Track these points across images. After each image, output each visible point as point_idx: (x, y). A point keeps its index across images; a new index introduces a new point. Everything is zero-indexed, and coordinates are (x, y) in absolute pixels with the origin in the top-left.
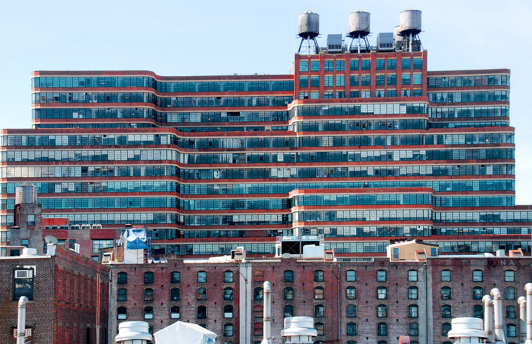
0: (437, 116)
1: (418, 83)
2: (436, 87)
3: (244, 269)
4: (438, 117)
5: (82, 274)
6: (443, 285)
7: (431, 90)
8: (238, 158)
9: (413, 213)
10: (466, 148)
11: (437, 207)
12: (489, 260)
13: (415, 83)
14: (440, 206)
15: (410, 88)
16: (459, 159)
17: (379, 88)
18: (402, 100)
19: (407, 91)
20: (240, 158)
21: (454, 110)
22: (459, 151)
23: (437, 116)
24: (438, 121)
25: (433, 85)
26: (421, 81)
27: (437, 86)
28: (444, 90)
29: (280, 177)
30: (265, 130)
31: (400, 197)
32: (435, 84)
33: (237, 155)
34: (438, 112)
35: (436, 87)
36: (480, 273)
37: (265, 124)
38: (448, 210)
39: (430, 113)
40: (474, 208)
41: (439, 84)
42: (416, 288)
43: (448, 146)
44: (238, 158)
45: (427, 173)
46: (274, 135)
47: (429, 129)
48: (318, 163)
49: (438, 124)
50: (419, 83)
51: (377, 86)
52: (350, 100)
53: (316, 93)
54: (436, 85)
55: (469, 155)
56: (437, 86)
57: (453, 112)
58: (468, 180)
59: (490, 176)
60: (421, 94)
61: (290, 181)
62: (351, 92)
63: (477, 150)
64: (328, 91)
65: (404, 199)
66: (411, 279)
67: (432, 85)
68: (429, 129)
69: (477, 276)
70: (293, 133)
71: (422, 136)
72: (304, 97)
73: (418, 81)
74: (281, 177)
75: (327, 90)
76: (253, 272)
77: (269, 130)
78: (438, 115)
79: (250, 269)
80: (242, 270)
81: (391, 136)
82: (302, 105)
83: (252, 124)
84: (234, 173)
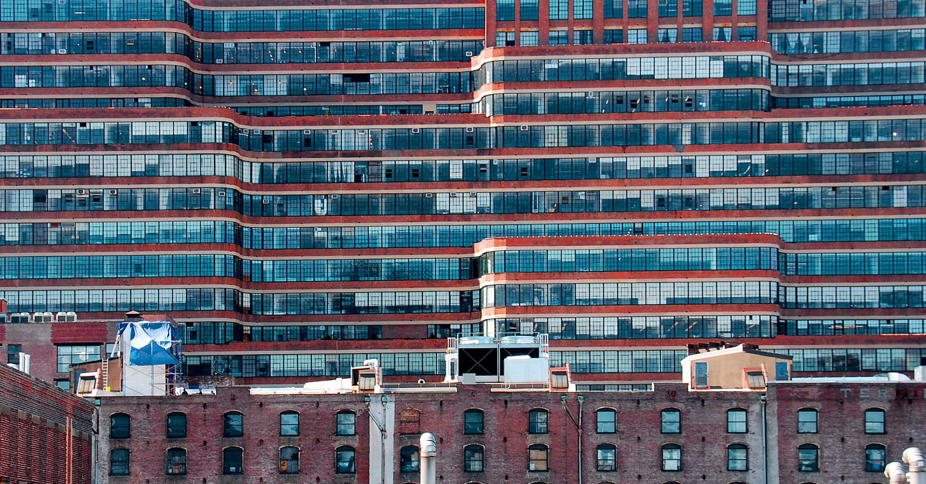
2: (786, 21)
3: (380, 407)
5: (36, 417)
6: (802, 440)
8: (366, 171)
9: (739, 288)
11: (790, 275)
12: (899, 387)
13: (742, 13)
14: (794, 273)
15: (731, 22)
20: (370, 172)
21: (824, 71)
22: (836, 158)
24: (791, 93)
25: (780, 16)
27: (788, 19)
29: (455, 212)
30: (424, 113)
31: (711, 253)
33: (364, 164)
34: (791, 74)
35: (786, 21)
36: (879, 416)
37: (424, 100)
41: (794, 15)
42: (745, 447)
44: (366, 171)
46: (442, 123)
47: (772, 110)
48: (536, 182)
51: (661, 20)
52: (603, 49)
56: (788, 19)
57: (822, 73)
58: (854, 217)
59: (901, 210)
60: (754, 36)
62: (606, 32)
63: (873, 155)
64: (558, 29)
65: (719, 259)
66: (733, 428)
69: (875, 423)
70: (483, 118)
71: (757, 124)
72: (506, 41)
73: (528, 38)
74: (458, 212)
75: (555, 27)
76: (398, 414)
77: (433, 112)
78: (790, 80)
79: (391, 407)
80: (375, 409)
82: (502, 58)
83: (397, 100)
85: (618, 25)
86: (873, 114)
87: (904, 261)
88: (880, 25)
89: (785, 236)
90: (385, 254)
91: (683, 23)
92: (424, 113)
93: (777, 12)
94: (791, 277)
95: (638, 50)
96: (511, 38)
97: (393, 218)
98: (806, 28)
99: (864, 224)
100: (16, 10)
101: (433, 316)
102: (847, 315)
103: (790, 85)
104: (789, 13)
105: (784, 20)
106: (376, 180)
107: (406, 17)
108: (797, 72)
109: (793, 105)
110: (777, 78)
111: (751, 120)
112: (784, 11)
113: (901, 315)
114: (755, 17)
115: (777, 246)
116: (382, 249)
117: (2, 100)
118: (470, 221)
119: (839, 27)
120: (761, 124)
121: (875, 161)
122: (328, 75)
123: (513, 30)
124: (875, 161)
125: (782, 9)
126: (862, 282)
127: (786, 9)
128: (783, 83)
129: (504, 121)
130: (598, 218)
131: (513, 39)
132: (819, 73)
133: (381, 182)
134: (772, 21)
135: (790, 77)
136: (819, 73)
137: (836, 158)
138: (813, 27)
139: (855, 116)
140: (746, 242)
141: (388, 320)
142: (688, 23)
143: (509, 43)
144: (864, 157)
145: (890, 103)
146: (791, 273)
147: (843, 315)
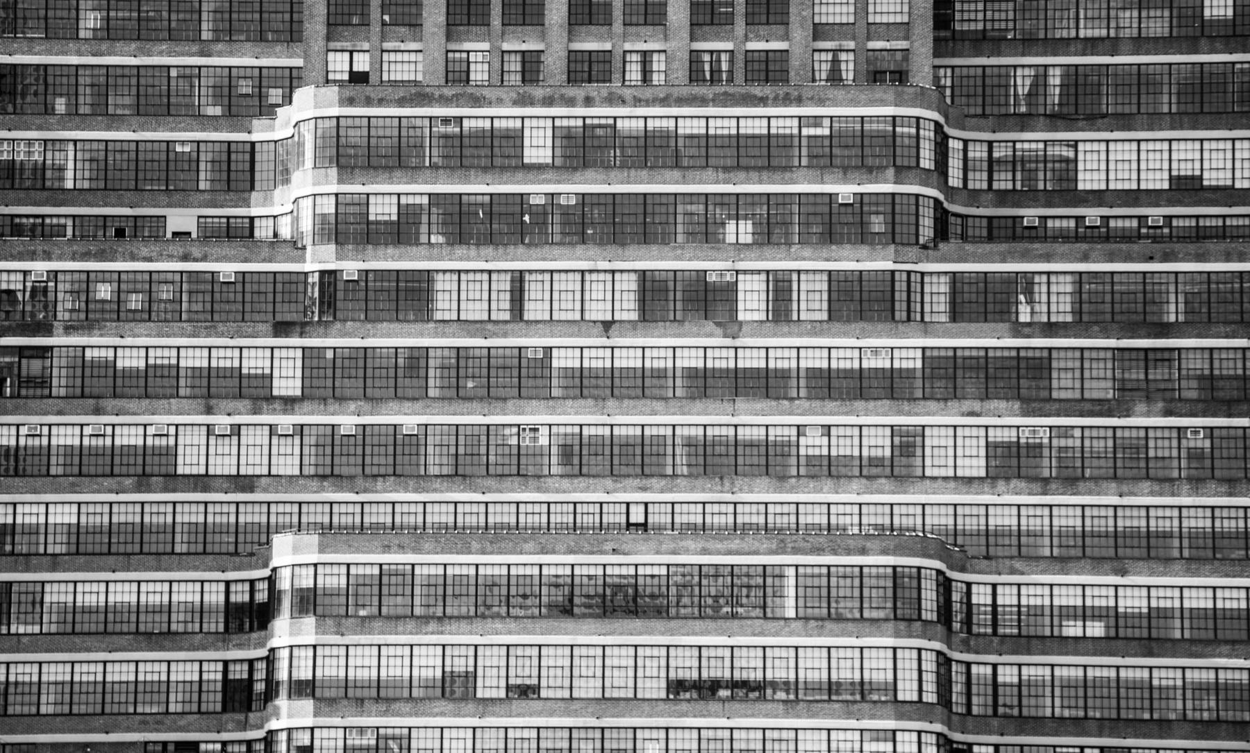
0: (990, 180)
1: (892, 19)
2: (984, 38)
4: (995, 186)
7: (961, 56)
8: (16, 371)
10: (1112, 343)
11: (979, 635)
13: (878, 19)
14: (989, 630)
15: (854, 38)
16: (1083, 399)
17: (705, 40)
18: (812, 99)
19: (843, 56)
20: (24, 373)
21: (1071, 155)
22: (1082, 359)
23: (990, 180)
24: (997, 206)
25: (973, 26)
26: (385, 67)
27: (989, 34)
28: (1023, 55)
29: (219, 472)
30: (169, 235)
32: (980, 26)
33: (12, 355)
34: (999, 161)
35: (984, 38)
37: (169, 206)
38: (1029, 653)
39: (955, 165)
40: (1154, 644)
41: (1003, 26)
43: (1026, 330)
44: (16, 371)
45: (834, 453)
46: (196, 260)
47: (941, 245)
48: (407, 404)
49: (995, 223)
50: (899, 19)
51: (698, 31)
52: (562, 96)
53: (406, 57)
54: (985, 30)
55: (1127, 376)
56: (989, 34)
57: (1067, 161)
58: (1127, 501)
61: (265, 490)
62: (573, 57)
63: (1166, 355)
64: (467, 46)
65: (801, 592)
67: (965, 27)
68: (941, 245)
70: (296, 246)
71: (904, 276)
72: (351, 72)
73: (399, 66)
74: (226, 472)
75: (460, 40)
77: (189, 234)
78: (996, 176)
81: (508, 277)
82: (336, 111)
83: (106, 205)
84: (1123, 691)
85: (601, 38)
86: (1166, 258)
87: (189, 311)
88: (1196, 52)
89: (968, 542)
90: (54, 568)
91: (747, 39)
92: (169, 235)
93: (966, 16)
94: (981, 640)
95: (640, 101)
96: (362, 63)
97: (73, 484)
98: (1029, 55)
99: (1148, 517)
100: (1134, 166)
101: (158, 723)
102: (1109, 736)
103: (995, 186)
104: (993, 20)
105: (980, 36)
106: (39, 392)
107: (131, 10)
108: (765, 131)
109: (977, 233)
110: (965, 170)
111: (889, 265)
112: (980, 16)
113: (1236, 739)
114: (905, 30)
115: (938, 564)
116: (45, 559)
117: (4, 745)
118: (252, 492)
119: (1104, 54)
120: (913, 275)
121: (1170, 368)
122: (1045, 354)
123: (366, 46)
124: (1170, 368)
125: (976, 11)
126: (1145, 656)
127: (985, 11)
128: (978, 181)
129: (337, 259)
130: (547, 491)
131: (367, 69)
132: (1061, 161)
133: (50, 396)
134: (954, 39)
135: (996, 168)
136: (1061, 161)
137: (1082, 359)
138: (1045, 54)
139: (1125, 261)
140: (863, 551)
141: (51, 731)
142: (759, 38)
143: (358, 78)
144: (1146, 359)
145: (1220, 233)
146: (982, 630)
147: (1100, 735)
